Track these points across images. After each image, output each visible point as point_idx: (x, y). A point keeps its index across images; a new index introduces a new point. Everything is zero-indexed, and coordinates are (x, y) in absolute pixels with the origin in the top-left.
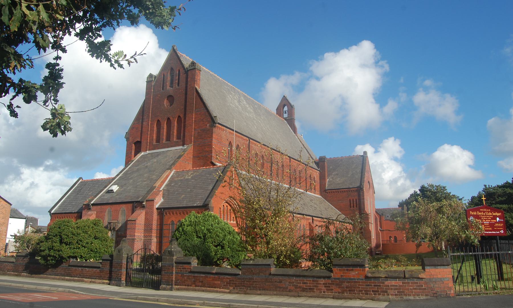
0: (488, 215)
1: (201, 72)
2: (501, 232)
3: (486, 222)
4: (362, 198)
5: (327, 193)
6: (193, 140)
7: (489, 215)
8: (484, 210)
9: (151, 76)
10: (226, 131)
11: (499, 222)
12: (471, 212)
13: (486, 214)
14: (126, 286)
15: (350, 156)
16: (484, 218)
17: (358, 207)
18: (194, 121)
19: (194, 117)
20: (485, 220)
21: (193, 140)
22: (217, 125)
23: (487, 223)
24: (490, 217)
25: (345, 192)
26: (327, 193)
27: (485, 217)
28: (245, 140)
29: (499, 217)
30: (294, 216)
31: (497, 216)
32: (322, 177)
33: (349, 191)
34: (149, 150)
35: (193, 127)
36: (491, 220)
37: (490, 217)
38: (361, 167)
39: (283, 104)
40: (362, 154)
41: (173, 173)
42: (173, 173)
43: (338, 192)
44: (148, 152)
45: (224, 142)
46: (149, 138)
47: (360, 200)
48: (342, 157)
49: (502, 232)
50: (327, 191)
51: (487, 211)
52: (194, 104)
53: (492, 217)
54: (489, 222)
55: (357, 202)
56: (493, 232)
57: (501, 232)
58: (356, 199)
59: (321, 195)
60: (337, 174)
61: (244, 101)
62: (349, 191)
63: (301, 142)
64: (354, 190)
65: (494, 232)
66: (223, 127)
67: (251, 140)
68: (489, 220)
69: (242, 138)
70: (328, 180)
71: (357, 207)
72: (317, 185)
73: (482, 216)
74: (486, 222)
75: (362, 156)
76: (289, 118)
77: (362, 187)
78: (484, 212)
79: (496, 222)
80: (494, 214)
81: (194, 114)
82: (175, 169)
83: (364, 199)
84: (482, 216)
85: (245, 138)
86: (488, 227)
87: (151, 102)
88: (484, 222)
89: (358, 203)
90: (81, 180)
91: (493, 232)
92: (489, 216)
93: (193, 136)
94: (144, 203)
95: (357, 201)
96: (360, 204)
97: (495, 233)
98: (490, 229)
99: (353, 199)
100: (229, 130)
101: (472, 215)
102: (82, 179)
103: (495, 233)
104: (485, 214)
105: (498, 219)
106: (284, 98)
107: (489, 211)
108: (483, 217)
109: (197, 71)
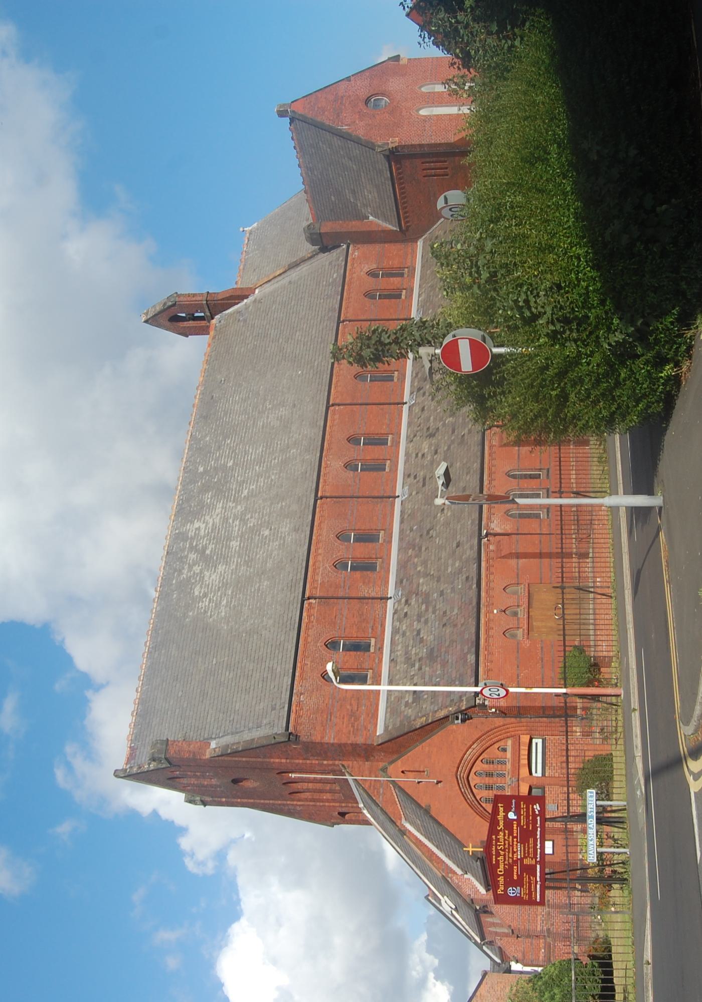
0: (505, 844)
1: (169, 739)
2: (537, 813)
3: (519, 853)
4: (418, 150)
5: (408, 227)
6: (331, 762)
7: (505, 840)
8: (494, 853)
9: (190, 801)
10: (301, 694)
11: (518, 813)
12: (499, 892)
13: (501, 849)
14: (624, 494)
15: (295, 148)
16: (511, 856)
17: (446, 159)
18: (288, 761)
19: (277, 760)
20: (513, 852)
21: (331, 762)
22: (291, 729)
23: (518, 848)
24: (509, 838)
25: (404, 188)
26: (408, 227)
27: (509, 852)
28: (309, 616)
29: (507, 811)
30: (487, 535)
31: (506, 817)
32: (369, 237)
33: (407, 217)
34: (357, 803)
35: (301, 761)
36: (513, 837)
37: (509, 838)
38: (328, 136)
39: (169, 323)
40: (287, 120)
41: (408, 826)
42: (408, 826)
43: (404, 203)
44: (361, 805)
45: (326, 702)
46: (331, 804)
47: (423, 155)
48: (299, 166)
49: (539, 809)
50: (404, 228)
51: (496, 845)
52: (248, 759)
53: (507, 832)
54: (517, 841)
55: (432, 160)
56: (538, 837)
57: (537, 813)
58: (423, 163)
59: (415, 240)
60: (353, 192)
61: (196, 525)
62: (405, 218)
63: (269, 281)
64: (397, 169)
65: (538, 833)
66: (293, 708)
67: (307, 595)
68: (513, 841)
69: (307, 628)
70: (371, 218)
71: (445, 162)
72: (394, 249)
73: (506, 862)
74: (519, 853)
75: (292, 120)
76: (207, 310)
77: (387, 153)
78: (498, 855)
79: (518, 820)
80: (501, 826)
81: (272, 760)
82: (401, 819)
83: (421, 146)
84: (506, 862)
85: (305, 614)
86: (529, 848)
87: (250, 801)
88: (519, 857)
89: (435, 159)
90: (430, 898)
91: (538, 837)
92: (507, 842)
93: (321, 762)
94: (478, 908)
95: (428, 160)
96: (437, 155)
97: (539, 829)
98: (531, 841)
99: (424, 176)
100: (296, 682)
101: (505, 890)
102: (428, 895)
103: (539, 829)
104: (502, 853)
105: (511, 815)
106: (153, 320)
107: (496, 837)
108: (509, 857)
109: (172, 752)
